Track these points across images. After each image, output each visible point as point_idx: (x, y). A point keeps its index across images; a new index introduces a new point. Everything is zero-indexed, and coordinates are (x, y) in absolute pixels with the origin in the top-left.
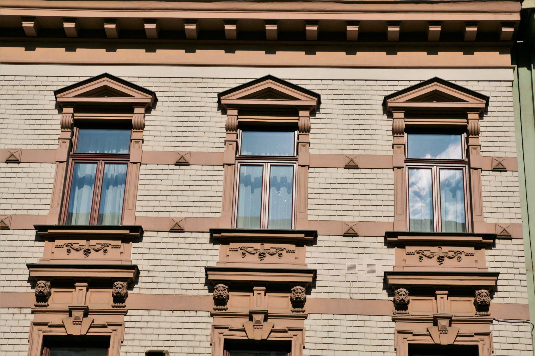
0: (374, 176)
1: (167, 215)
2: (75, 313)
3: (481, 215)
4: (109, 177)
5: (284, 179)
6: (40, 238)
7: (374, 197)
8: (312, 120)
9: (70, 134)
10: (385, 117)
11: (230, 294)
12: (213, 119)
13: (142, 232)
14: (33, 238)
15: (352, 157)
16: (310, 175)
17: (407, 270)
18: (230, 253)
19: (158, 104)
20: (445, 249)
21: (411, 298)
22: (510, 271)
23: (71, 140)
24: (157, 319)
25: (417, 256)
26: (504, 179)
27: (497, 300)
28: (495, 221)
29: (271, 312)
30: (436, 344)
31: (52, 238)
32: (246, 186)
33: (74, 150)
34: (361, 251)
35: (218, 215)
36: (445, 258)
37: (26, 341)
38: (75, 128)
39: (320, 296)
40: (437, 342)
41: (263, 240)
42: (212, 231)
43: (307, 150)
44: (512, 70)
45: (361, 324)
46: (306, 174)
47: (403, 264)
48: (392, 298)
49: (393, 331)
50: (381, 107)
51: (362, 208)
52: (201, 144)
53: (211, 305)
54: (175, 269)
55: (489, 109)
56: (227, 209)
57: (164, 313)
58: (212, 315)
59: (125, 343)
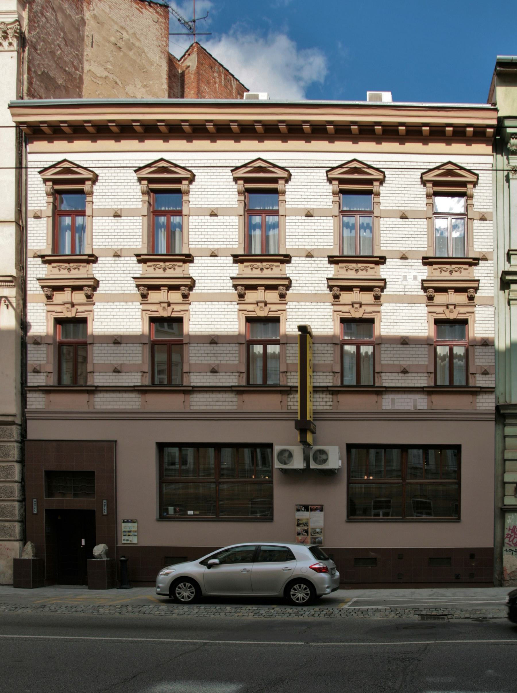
0: (416, 223)
1: (303, 247)
2: (260, 304)
3: (473, 246)
4: (270, 223)
5: (368, 224)
6: (235, 262)
7: (416, 236)
8: (381, 188)
9: (338, 198)
10: (422, 186)
11: (341, 293)
12: (325, 187)
13: (291, 258)
14: (232, 261)
15: (404, 211)
16: (381, 223)
17: (433, 278)
18: (340, 270)
19: (292, 177)
20: (454, 266)
21: (435, 294)
22: (486, 278)
23: (244, 201)
24: (303, 307)
25: (439, 270)
26: (485, 225)
27: (479, 294)
28: (479, 250)
29: (363, 302)
30: (448, 319)
31: (242, 262)
32: (347, 228)
33: (248, 207)
34: (409, 267)
35: (332, 247)
36: (454, 272)
37: (236, 320)
38: (246, 194)
39: (389, 293)
40: (448, 317)
41: (357, 262)
42: (329, 257)
43: (379, 207)
44: (492, 157)
45: (410, 308)
46: (379, 221)
47: (432, 275)
48: (426, 294)
49: (426, 312)
50: (420, 180)
51: (410, 242)
52: (319, 203)
53: (331, 299)
54: (310, 279)
55: (479, 181)
56: (430, 245)
57: (307, 304)
58: (332, 305)
59: (288, 320)
